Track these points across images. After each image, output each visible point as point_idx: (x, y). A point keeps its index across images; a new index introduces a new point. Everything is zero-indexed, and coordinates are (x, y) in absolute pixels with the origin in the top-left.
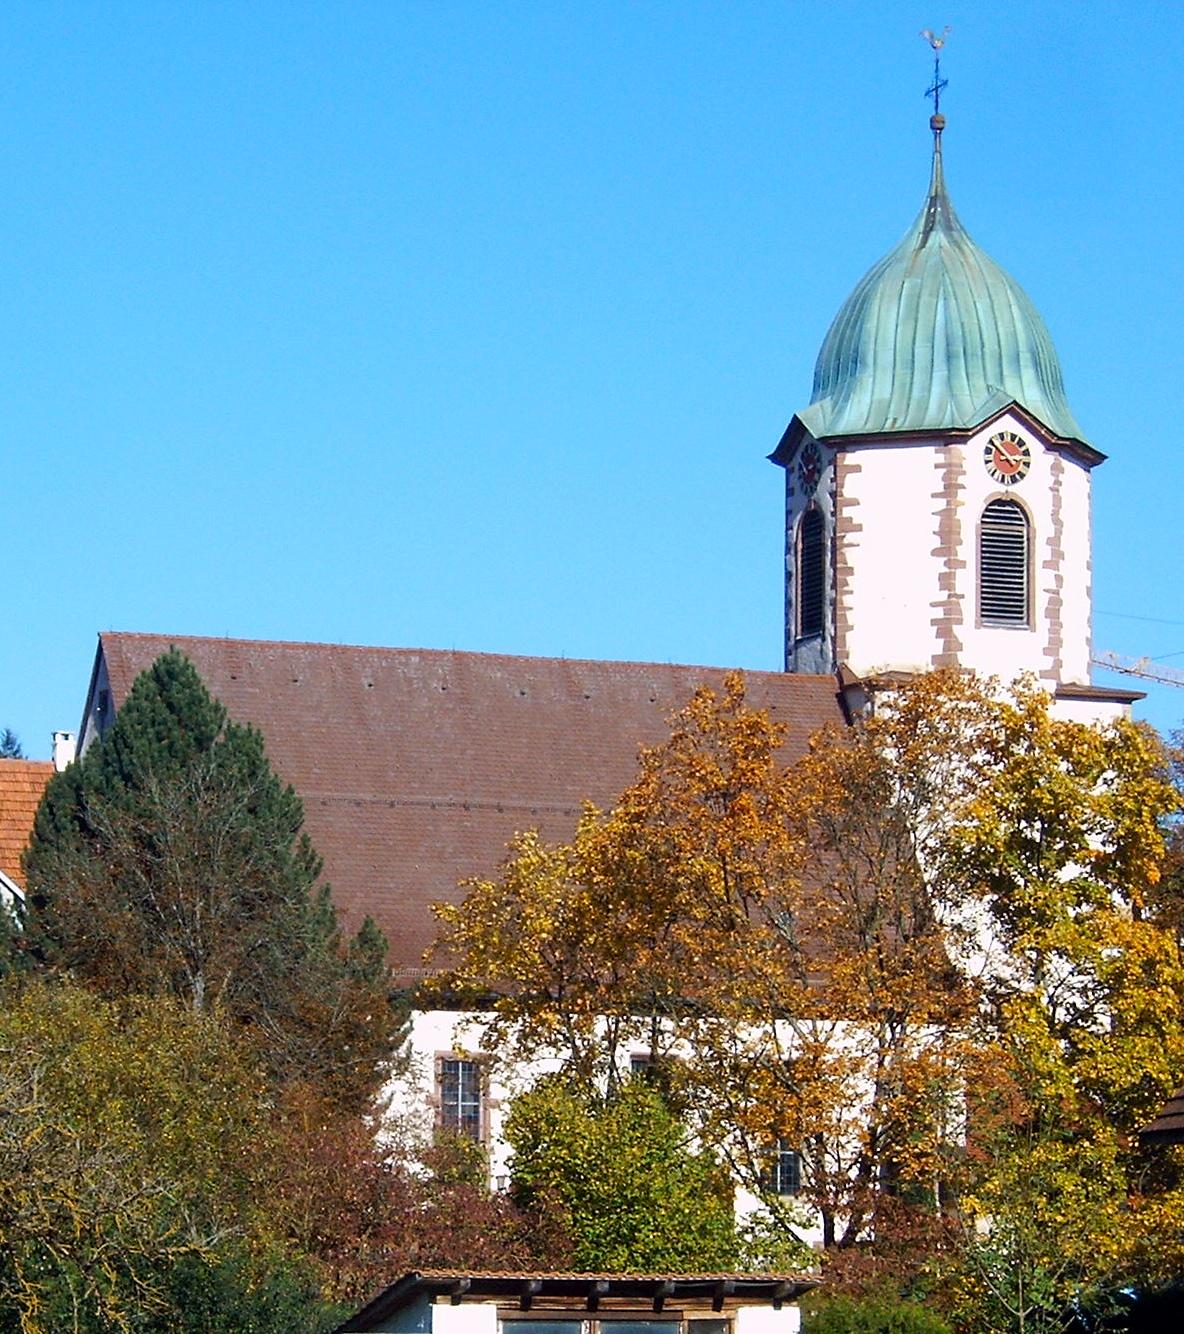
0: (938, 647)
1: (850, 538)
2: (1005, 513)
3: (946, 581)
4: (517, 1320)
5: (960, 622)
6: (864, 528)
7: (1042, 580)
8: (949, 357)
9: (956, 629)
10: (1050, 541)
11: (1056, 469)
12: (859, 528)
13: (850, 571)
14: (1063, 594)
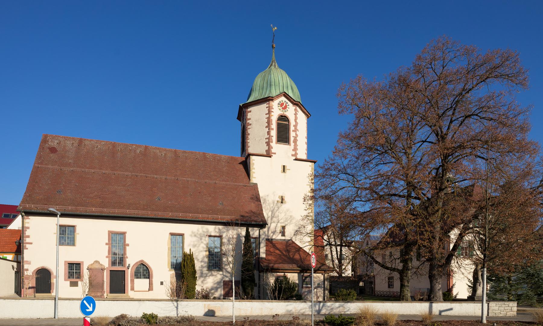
0: (267, 148)
1: (249, 127)
2: (283, 118)
3: (269, 133)
4: (332, 256)
5: (272, 142)
6: (283, 174)
7: (292, 134)
8: (270, 85)
9: (271, 143)
10: (294, 126)
11: (296, 110)
12: (251, 124)
13: (249, 134)
14: (298, 138)
